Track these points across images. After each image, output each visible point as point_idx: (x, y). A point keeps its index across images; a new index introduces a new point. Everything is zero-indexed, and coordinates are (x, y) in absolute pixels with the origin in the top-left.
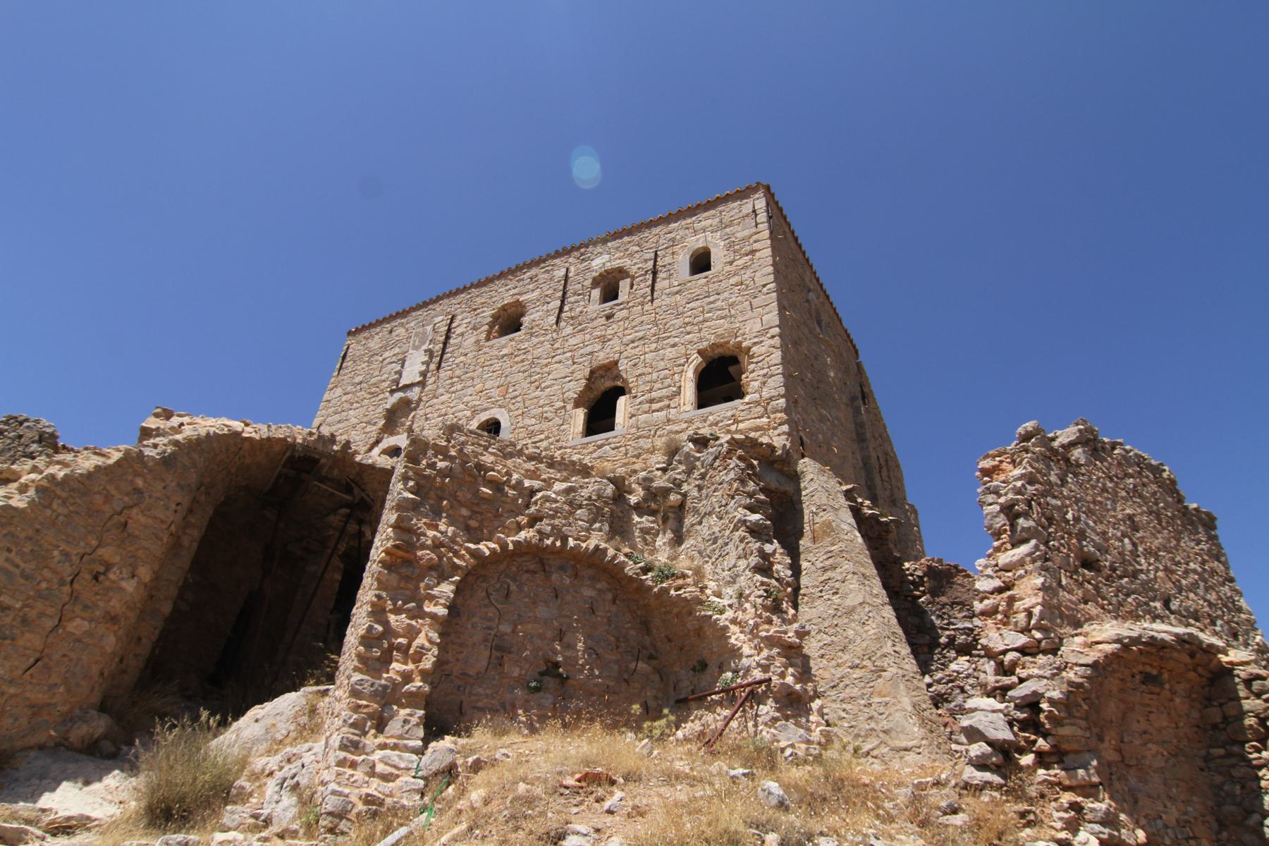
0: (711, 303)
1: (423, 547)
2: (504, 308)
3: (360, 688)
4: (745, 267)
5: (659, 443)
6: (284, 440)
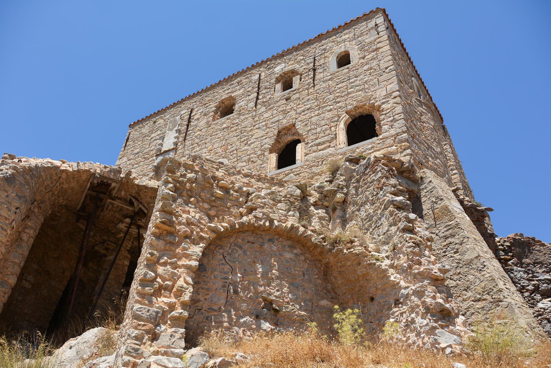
0: (352, 83)
1: (180, 223)
2: (222, 102)
3: (140, 313)
4: (373, 59)
5: (325, 168)
6: (88, 171)
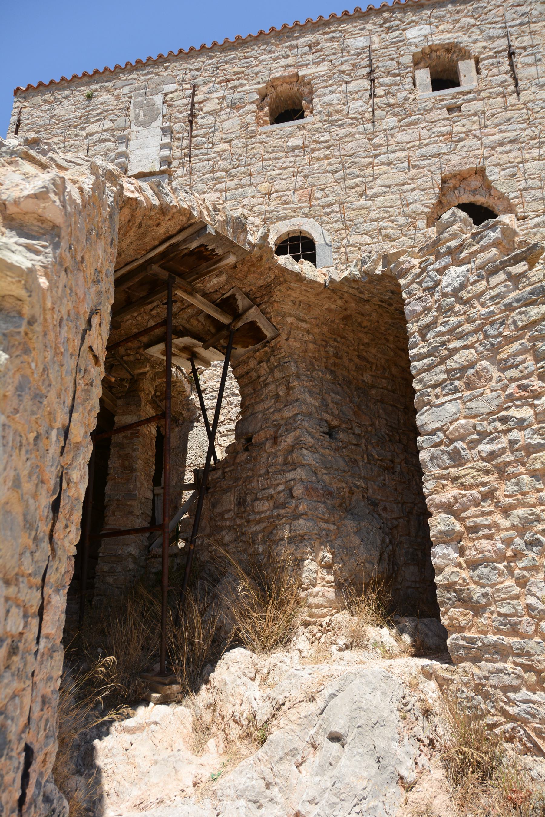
2: (272, 84)
